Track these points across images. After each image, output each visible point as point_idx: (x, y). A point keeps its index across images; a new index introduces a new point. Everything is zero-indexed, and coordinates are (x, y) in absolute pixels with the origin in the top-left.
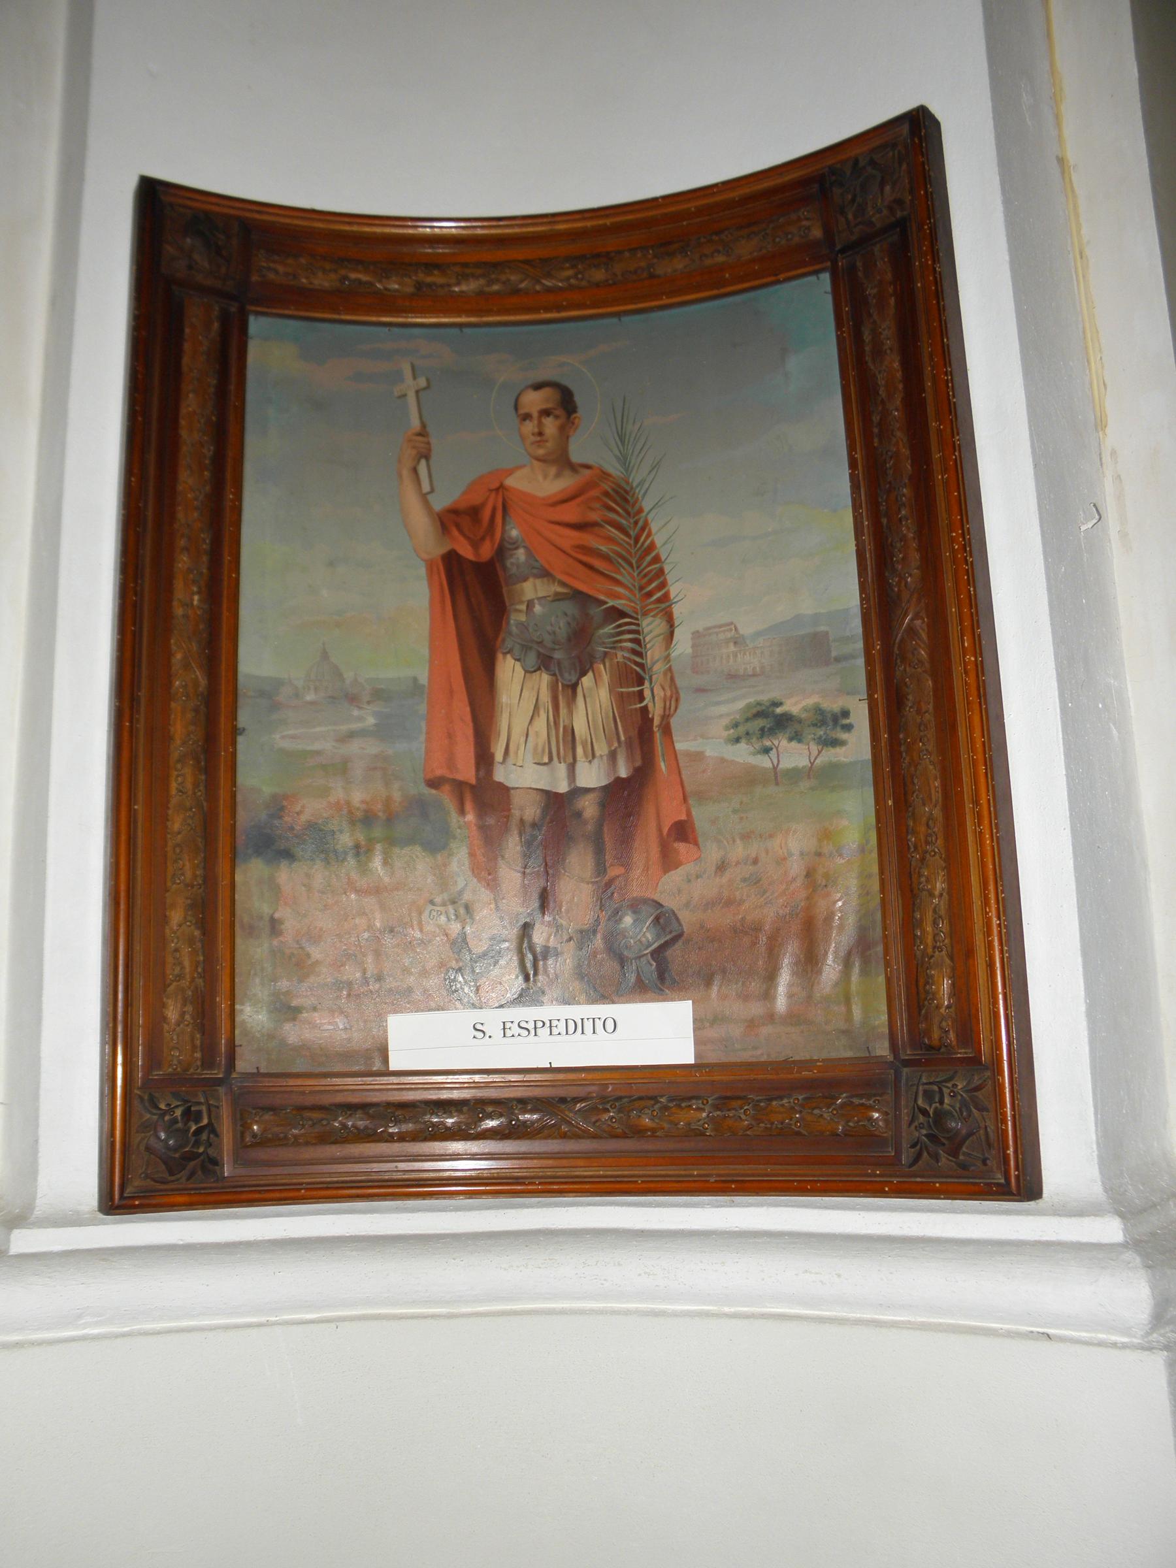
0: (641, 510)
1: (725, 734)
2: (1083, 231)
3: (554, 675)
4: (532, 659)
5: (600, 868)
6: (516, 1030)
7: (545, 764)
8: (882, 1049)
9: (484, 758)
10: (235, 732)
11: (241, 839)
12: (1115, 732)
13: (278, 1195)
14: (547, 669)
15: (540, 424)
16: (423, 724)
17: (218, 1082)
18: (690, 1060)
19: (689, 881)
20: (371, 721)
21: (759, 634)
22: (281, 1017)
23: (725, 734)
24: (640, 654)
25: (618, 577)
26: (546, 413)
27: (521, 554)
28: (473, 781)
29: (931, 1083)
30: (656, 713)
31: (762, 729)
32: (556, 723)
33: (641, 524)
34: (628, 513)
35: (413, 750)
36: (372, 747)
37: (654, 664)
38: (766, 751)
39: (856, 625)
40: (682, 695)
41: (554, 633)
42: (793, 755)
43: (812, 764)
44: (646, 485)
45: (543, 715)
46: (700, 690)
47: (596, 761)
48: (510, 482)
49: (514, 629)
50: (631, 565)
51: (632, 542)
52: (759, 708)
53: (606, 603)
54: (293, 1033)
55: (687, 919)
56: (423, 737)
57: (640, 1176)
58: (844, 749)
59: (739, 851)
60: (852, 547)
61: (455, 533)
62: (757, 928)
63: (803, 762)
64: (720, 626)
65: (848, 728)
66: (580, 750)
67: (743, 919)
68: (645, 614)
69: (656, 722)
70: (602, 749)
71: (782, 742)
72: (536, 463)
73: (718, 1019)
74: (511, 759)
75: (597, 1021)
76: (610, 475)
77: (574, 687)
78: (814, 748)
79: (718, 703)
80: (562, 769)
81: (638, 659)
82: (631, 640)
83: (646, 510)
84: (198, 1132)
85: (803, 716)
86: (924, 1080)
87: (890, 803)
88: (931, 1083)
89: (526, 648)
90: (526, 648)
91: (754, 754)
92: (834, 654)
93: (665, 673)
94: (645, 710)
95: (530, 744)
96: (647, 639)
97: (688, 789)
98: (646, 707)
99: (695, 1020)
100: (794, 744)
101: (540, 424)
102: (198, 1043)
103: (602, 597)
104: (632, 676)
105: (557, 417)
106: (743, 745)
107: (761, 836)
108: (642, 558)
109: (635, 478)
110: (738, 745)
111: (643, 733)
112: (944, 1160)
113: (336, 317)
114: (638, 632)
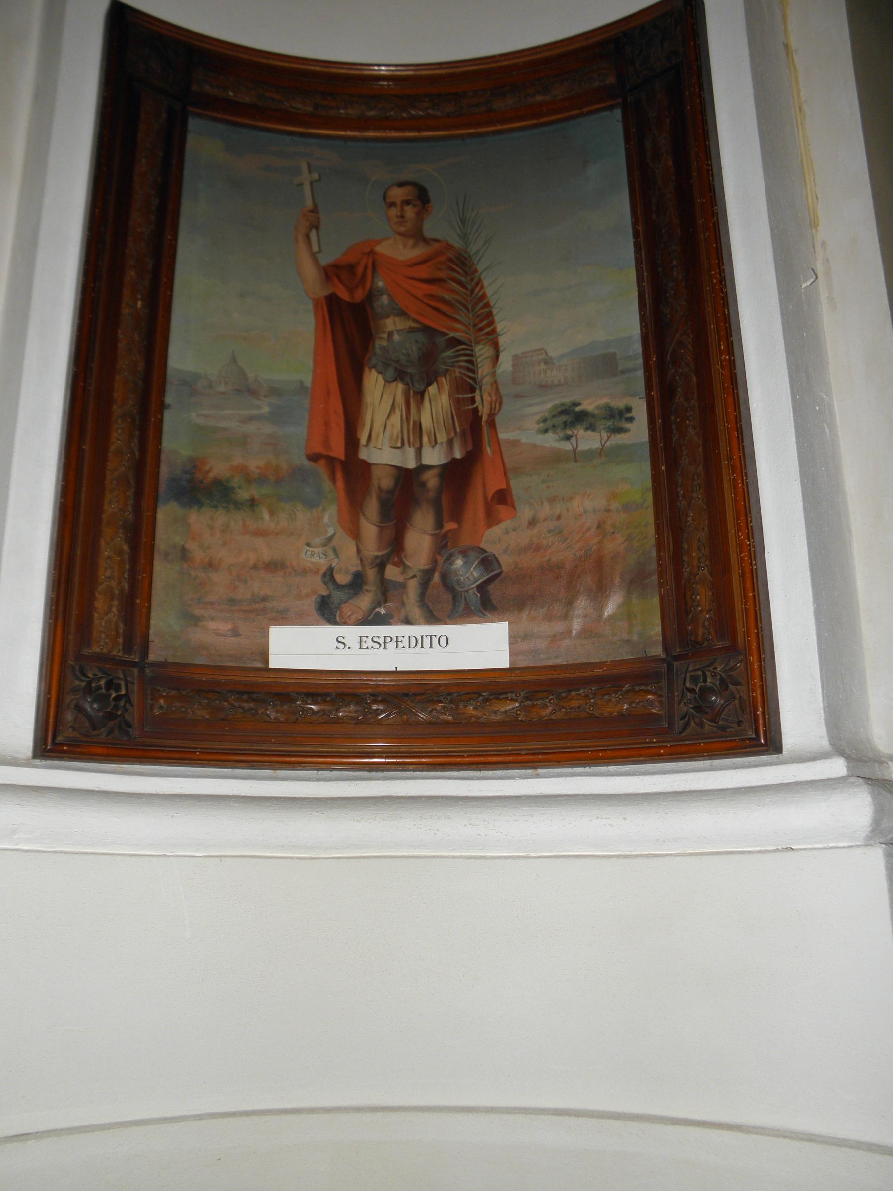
0: (476, 271)
1: (537, 427)
2: (802, 93)
3: (407, 384)
4: (391, 372)
5: (439, 524)
6: (370, 643)
7: (398, 448)
8: (657, 651)
9: (352, 442)
10: (162, 406)
11: (163, 487)
12: (827, 430)
13: (177, 756)
14: (402, 380)
15: (402, 210)
16: (306, 414)
17: (134, 664)
18: (504, 662)
19: (507, 533)
20: (266, 410)
21: (562, 356)
22: (183, 627)
23: (537, 427)
24: (473, 372)
25: (458, 317)
26: (407, 203)
27: (385, 299)
28: (343, 457)
29: (696, 670)
30: (484, 412)
31: (565, 423)
32: (408, 419)
33: (476, 280)
34: (467, 273)
35: (297, 435)
36: (268, 429)
37: (483, 378)
38: (568, 438)
39: (637, 347)
40: (504, 399)
41: (408, 355)
42: (588, 440)
43: (603, 446)
44: (481, 254)
45: (398, 413)
46: (518, 396)
47: (437, 446)
48: (378, 249)
49: (378, 351)
50: (468, 309)
51: (469, 293)
52: (563, 408)
53: (447, 335)
54: (197, 636)
55: (506, 562)
56: (306, 423)
57: (465, 752)
58: (627, 434)
59: (546, 510)
60: (635, 294)
61: (336, 281)
62: (560, 566)
63: (596, 445)
64: (536, 351)
65: (631, 420)
66: (425, 439)
67: (549, 560)
68: (478, 343)
69: (484, 418)
70: (442, 437)
71: (580, 432)
72: (399, 237)
73: (526, 637)
74: (372, 444)
75: (433, 638)
76: (453, 247)
77: (421, 394)
78: (605, 435)
79: (530, 405)
80: (411, 452)
81: (471, 375)
82: (466, 361)
83: (480, 271)
84: (118, 698)
85: (596, 412)
86: (690, 669)
87: (663, 468)
88: (696, 670)
89: (386, 365)
90: (386, 365)
91: (558, 441)
92: (620, 368)
93: (492, 385)
94: (476, 410)
95: (387, 434)
96: (479, 360)
97: (509, 466)
98: (476, 409)
99: (510, 637)
100: (589, 432)
101: (402, 210)
102: (121, 631)
103: (445, 331)
104: (466, 387)
105: (415, 206)
106: (550, 434)
107: (563, 499)
108: (476, 304)
109: (472, 249)
110: (547, 435)
111: (473, 427)
112: (709, 727)
113: (253, 123)
114: (471, 356)
